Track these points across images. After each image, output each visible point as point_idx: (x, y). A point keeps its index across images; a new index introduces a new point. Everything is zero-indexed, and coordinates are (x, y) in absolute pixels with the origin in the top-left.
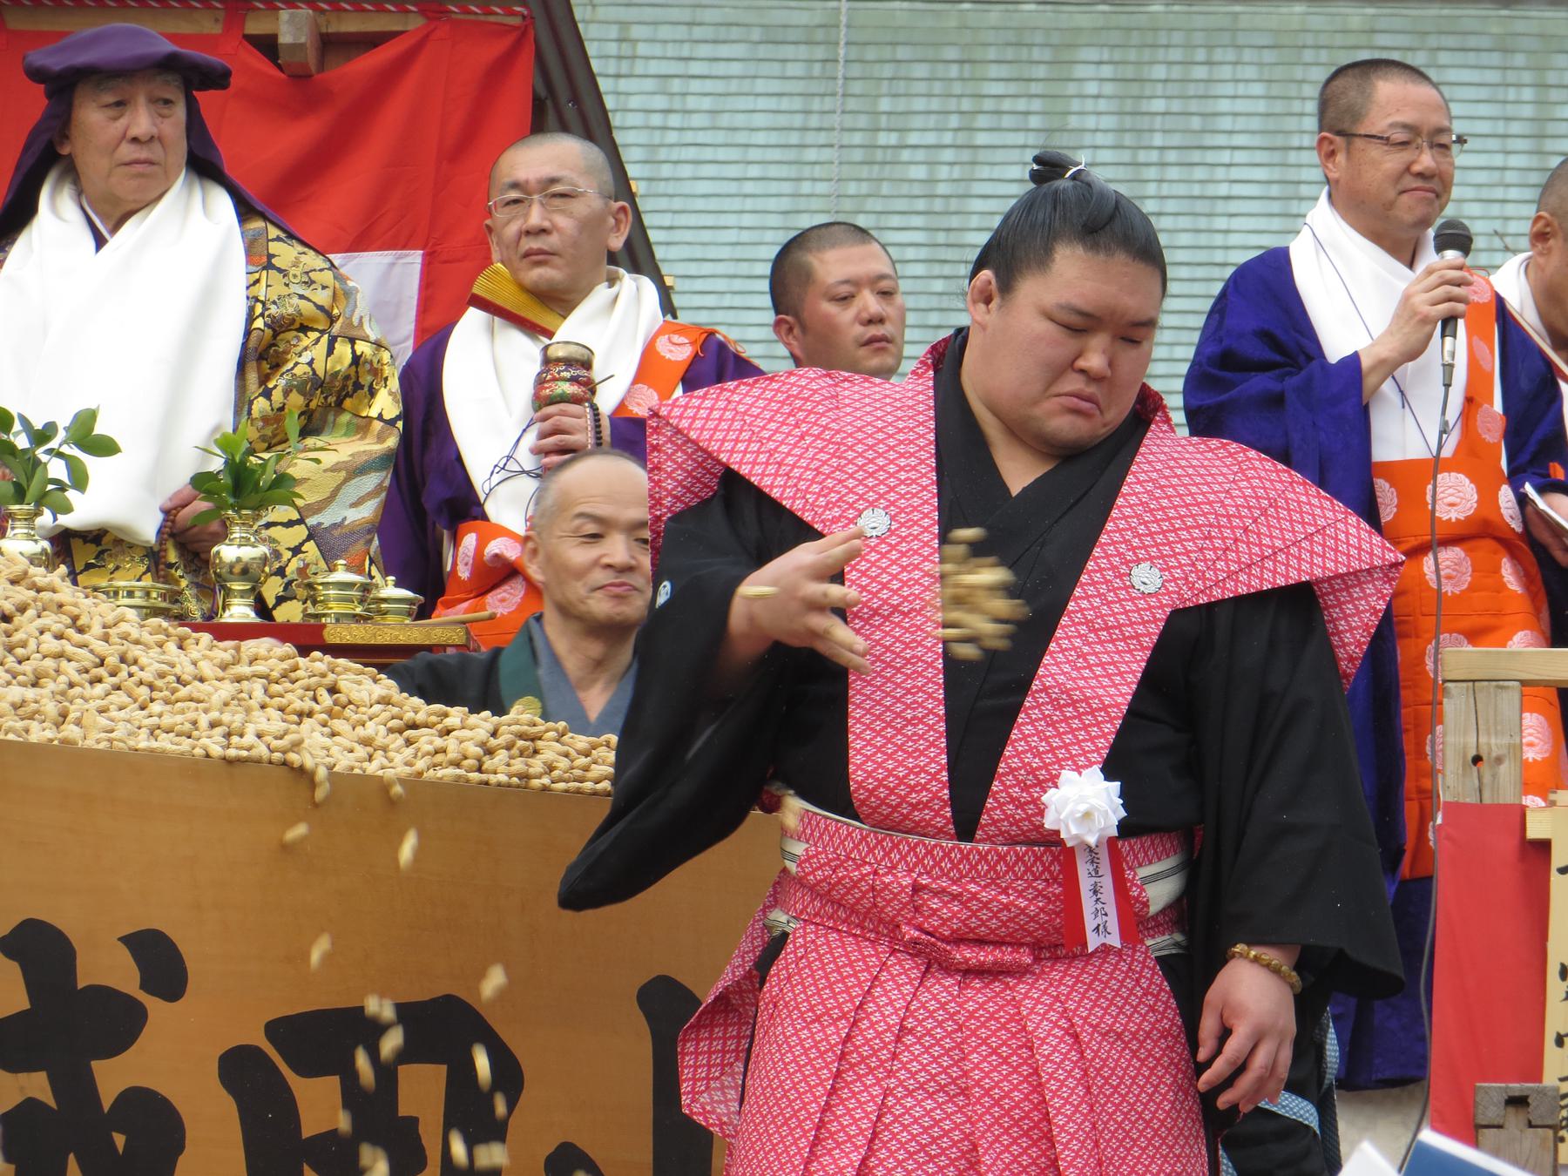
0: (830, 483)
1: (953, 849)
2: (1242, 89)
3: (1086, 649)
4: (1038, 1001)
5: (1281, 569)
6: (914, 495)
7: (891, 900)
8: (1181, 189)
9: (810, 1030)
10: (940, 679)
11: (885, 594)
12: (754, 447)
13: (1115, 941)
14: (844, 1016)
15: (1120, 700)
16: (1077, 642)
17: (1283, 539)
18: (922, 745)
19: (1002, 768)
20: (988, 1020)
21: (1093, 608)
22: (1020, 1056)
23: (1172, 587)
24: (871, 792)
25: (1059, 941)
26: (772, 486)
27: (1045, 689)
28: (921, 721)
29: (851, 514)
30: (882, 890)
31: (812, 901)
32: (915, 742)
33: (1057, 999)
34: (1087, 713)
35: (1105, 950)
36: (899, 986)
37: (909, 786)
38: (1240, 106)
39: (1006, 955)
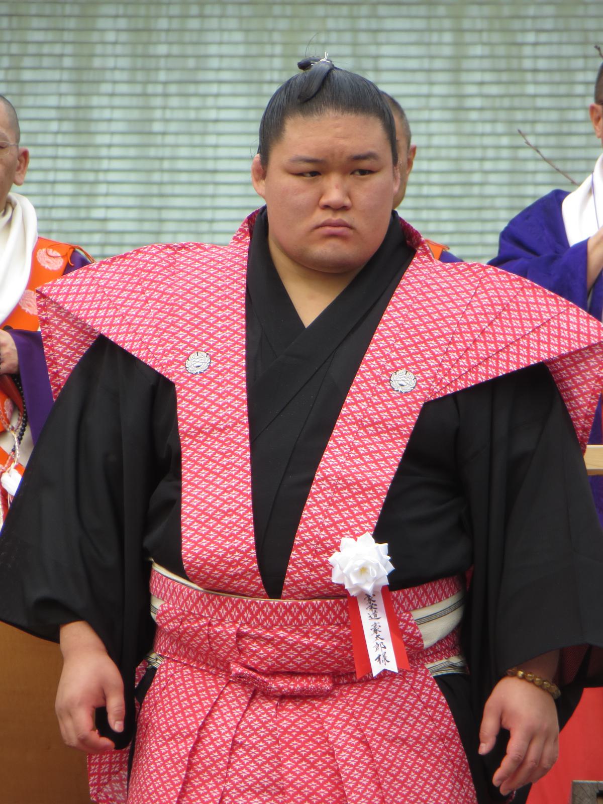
0: (166, 336)
1: (264, 604)
2: (226, 37)
3: (357, 443)
4: (337, 718)
5: (513, 358)
6: (228, 338)
7: (222, 645)
8: (180, 114)
9: (168, 745)
10: (249, 479)
11: (206, 416)
12: (111, 312)
13: (393, 667)
14: (190, 734)
15: (384, 479)
16: (350, 438)
17: (514, 335)
18: (236, 530)
19: (297, 541)
20: (299, 734)
21: (361, 410)
22: (324, 761)
23: (423, 385)
24: (200, 569)
25: (346, 670)
26: (124, 342)
27: (326, 478)
28: (234, 512)
29: (181, 357)
30: (215, 638)
31: (171, 644)
32: (230, 528)
33: (352, 715)
34: (359, 493)
35: (385, 674)
36: (231, 709)
37: (227, 563)
38: (225, 50)
39: (311, 684)
